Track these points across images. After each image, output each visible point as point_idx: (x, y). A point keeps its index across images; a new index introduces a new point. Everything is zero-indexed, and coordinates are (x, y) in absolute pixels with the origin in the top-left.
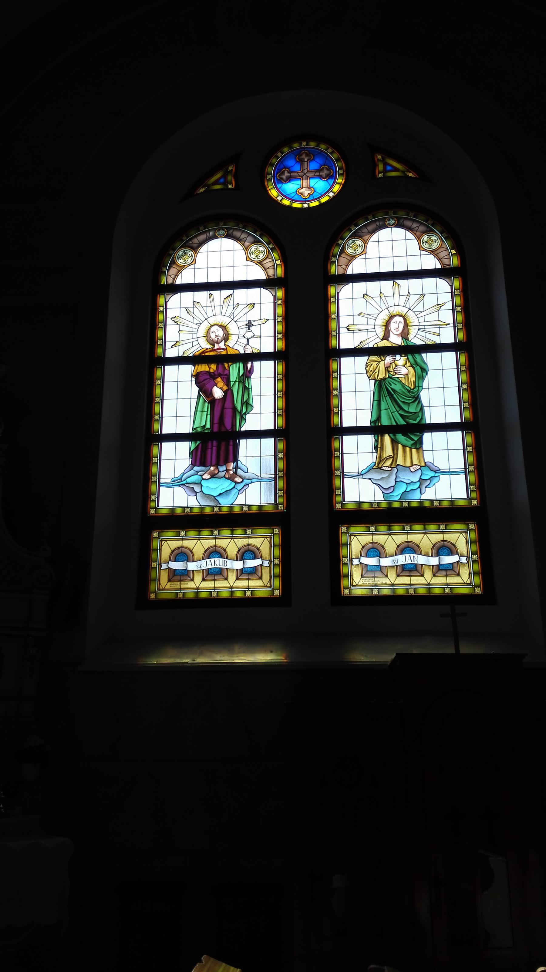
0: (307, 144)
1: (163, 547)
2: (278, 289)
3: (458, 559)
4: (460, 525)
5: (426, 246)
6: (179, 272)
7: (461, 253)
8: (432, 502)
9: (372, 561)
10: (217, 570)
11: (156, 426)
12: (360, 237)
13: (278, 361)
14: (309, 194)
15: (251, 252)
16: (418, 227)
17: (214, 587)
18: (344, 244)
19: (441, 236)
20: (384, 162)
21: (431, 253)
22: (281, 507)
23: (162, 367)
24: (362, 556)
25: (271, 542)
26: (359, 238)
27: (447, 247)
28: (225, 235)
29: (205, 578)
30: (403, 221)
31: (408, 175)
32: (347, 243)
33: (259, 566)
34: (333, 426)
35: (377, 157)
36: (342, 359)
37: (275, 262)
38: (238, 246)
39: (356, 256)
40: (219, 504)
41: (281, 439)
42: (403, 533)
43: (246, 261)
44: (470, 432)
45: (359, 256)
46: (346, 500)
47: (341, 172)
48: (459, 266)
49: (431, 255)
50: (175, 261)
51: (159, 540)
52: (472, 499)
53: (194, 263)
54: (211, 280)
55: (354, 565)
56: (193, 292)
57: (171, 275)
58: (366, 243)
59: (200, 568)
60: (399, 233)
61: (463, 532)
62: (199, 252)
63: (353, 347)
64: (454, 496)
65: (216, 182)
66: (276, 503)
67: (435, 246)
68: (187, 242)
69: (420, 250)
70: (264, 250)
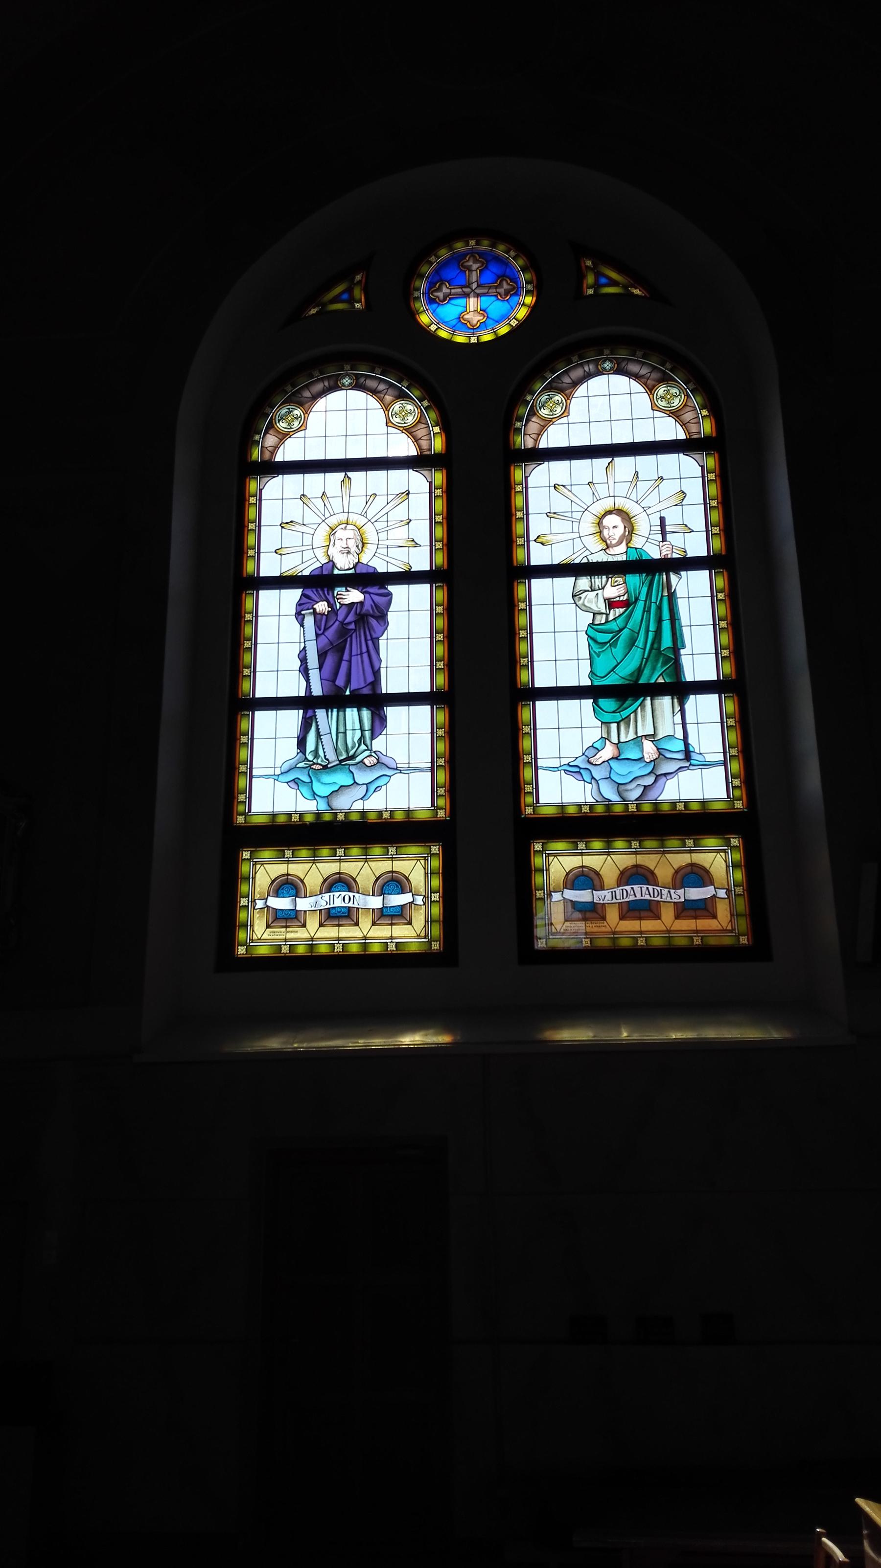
0: (477, 244)
1: (257, 874)
2: (436, 472)
3: (411, 900)
4: (417, 847)
5: (662, 404)
6: (543, 428)
7: (716, 413)
8: (674, 804)
9: (282, 903)
10: (343, 910)
11: (246, 686)
12: (561, 391)
13: (437, 585)
14: (479, 321)
15: (414, 414)
16: (386, 391)
17: (286, 939)
18: (534, 400)
19: (686, 388)
20: (596, 271)
21: (670, 414)
22: (441, 814)
23: (255, 592)
24: (270, 896)
25: (727, 860)
26: (299, 406)
27: (694, 406)
28: (353, 385)
29: (324, 923)
30: (365, 380)
31: (633, 293)
32: (538, 402)
33: (408, 904)
34: (519, 687)
35: (585, 263)
36: (533, 581)
37: (431, 429)
38: (373, 402)
39: (554, 420)
40: (330, 809)
41: (442, 707)
42: (603, 853)
43: (386, 427)
44: (443, 706)
45: (394, 426)
46: (541, 801)
47: (530, 287)
48: (714, 435)
49: (670, 418)
50: (536, 411)
51: (252, 863)
52: (735, 799)
53: (303, 428)
54: (310, 457)
55: (257, 909)
56: (302, 474)
57: (531, 434)
58: (306, 413)
59: (315, 907)
60: (621, 382)
61: (421, 858)
62: (312, 410)
63: (278, 574)
64: (708, 796)
65: (336, 300)
66: (434, 807)
67: (676, 403)
68: (293, 394)
69: (652, 409)
70: (414, 410)
